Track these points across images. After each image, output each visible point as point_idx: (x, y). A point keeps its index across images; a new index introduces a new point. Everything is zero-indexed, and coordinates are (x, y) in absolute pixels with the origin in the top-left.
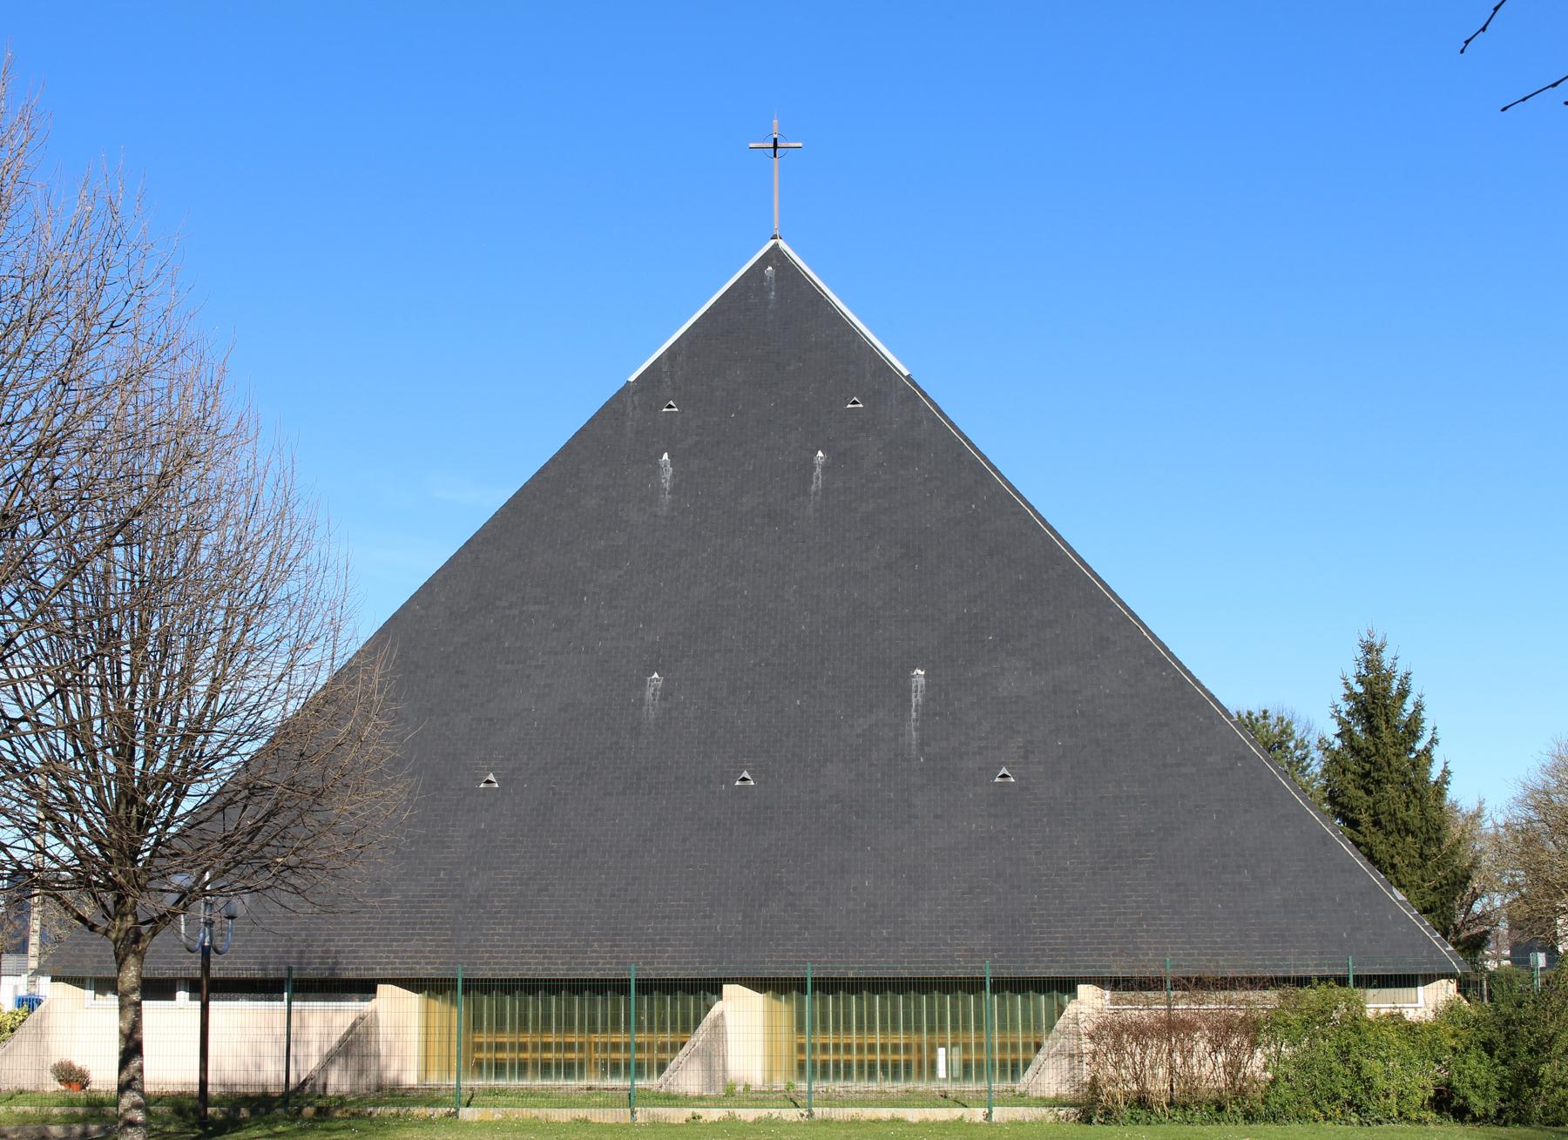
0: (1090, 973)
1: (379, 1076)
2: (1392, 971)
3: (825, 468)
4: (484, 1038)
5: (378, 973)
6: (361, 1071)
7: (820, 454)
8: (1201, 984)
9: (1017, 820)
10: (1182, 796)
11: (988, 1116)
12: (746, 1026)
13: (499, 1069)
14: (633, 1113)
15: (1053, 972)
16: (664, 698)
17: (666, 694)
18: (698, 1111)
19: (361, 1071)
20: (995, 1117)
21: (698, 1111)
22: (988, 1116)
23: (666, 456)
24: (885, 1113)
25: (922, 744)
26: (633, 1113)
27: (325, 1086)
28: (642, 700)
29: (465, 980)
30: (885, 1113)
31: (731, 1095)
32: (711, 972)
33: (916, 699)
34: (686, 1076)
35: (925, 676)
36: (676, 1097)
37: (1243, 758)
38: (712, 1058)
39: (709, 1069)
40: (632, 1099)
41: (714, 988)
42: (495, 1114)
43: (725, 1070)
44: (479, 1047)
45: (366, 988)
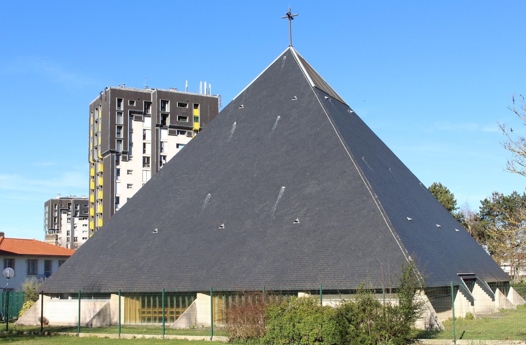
0: (201, 290)
1: (110, 321)
2: (331, 288)
3: (279, 121)
4: (145, 310)
5: (110, 291)
6: (104, 320)
7: (279, 117)
8: (326, 292)
9: (295, 236)
10: (350, 225)
11: (211, 339)
12: (203, 307)
13: (149, 320)
14: (119, 335)
15: (288, 288)
16: (209, 202)
17: (210, 200)
18: (136, 335)
19: (104, 320)
20: (213, 340)
21: (136, 335)
22: (211, 339)
23: (235, 123)
24: (183, 337)
25: (277, 211)
26: (119, 335)
27: (92, 325)
28: (203, 203)
29: (165, 293)
30: (183, 337)
31: (193, 330)
32: (296, 288)
33: (280, 197)
34: (181, 323)
35: (285, 189)
36: (176, 330)
37: (374, 211)
38: (190, 318)
39: (189, 320)
40: (164, 330)
41: (193, 295)
42: (87, 335)
43: (196, 320)
44: (143, 313)
45: (107, 296)
